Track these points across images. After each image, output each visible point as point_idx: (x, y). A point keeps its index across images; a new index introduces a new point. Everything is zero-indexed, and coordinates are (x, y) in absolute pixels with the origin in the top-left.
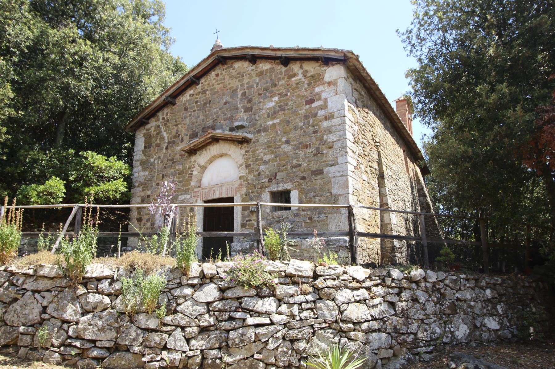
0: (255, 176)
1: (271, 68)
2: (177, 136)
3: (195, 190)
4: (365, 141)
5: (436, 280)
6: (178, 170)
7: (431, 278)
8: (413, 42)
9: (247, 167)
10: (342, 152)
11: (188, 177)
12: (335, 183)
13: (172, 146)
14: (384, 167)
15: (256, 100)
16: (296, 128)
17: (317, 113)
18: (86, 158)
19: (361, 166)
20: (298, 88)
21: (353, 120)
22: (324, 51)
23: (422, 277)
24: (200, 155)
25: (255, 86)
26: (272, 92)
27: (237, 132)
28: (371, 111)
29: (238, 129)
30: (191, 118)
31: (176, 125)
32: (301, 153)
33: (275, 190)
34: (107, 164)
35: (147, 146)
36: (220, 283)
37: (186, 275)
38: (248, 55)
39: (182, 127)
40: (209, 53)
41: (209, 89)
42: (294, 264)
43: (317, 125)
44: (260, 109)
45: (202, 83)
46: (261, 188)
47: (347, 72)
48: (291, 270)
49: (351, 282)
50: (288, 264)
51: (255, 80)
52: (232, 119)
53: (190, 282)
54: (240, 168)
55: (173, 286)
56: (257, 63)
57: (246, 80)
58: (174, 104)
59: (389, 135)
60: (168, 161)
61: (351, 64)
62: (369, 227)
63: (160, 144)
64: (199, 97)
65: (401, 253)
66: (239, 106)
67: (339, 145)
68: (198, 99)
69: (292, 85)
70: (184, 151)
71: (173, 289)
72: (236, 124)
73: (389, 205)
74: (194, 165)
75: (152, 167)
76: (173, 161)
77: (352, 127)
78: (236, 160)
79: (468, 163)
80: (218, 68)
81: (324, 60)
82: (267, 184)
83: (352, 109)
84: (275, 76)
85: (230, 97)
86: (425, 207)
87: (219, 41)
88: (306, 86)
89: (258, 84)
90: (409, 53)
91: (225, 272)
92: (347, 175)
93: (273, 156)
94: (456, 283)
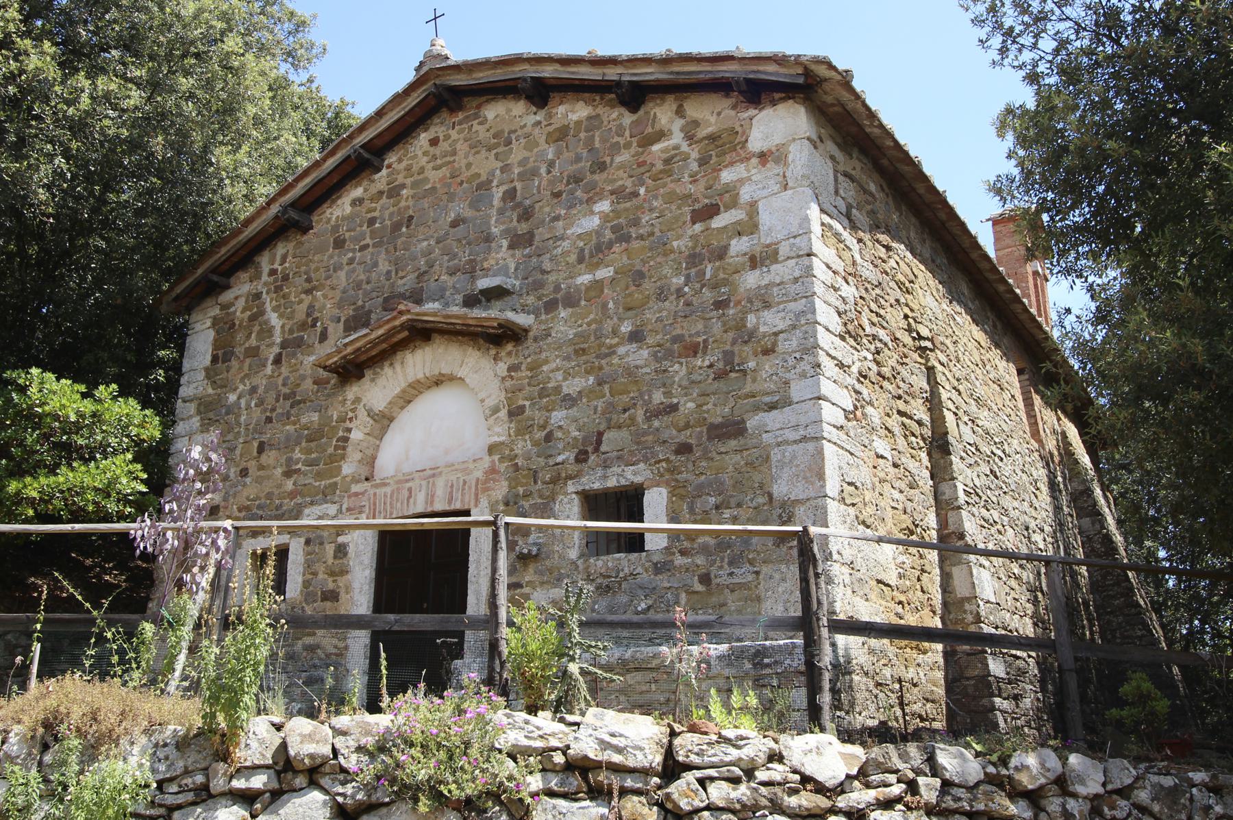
0: (536, 443)
1: (589, 118)
2: (309, 322)
3: (355, 488)
4: (882, 334)
5: (1101, 790)
7: (1082, 782)
8: (1008, 23)
9: (511, 414)
10: (804, 366)
11: (336, 448)
12: (782, 465)
13: (294, 355)
14: (949, 417)
15: (544, 210)
16: (661, 295)
17: (726, 248)
18: (23, 390)
19: (869, 410)
20: (669, 173)
21: (839, 265)
22: (744, 60)
23: (1051, 776)
24: (373, 380)
25: (543, 171)
26: (591, 187)
27: (486, 308)
28: (900, 241)
29: (488, 300)
30: (354, 271)
31: (308, 292)
32: (678, 371)
33: (596, 486)
34: (88, 406)
35: (222, 355)
36: (340, 789)
37: (225, 760)
38: (524, 79)
39: (325, 296)
40: (410, 76)
41: (408, 181)
42: (598, 724)
43: (725, 282)
44: (557, 239)
45: (389, 167)
46: (555, 480)
47: (818, 124)
48: (585, 746)
49: (794, 792)
50: (578, 724)
51: (543, 153)
52: (472, 270)
53: (238, 784)
54: (492, 420)
55: (181, 799)
56: (550, 104)
57: (517, 153)
58: (305, 229)
59: (964, 319)
60: (277, 400)
61: (829, 99)
62: (899, 609)
63: (258, 348)
64: (378, 206)
65: (1016, 698)
66: (494, 230)
67: (794, 343)
68: (376, 214)
69: (653, 165)
70: (325, 368)
71: (179, 807)
72: (484, 283)
73: (968, 539)
74: (353, 410)
75: (231, 418)
76: (295, 400)
77: (836, 290)
78: (482, 395)
79: (1198, 388)
80: (437, 121)
81: (744, 87)
82: (572, 468)
83: (837, 235)
84: (603, 141)
85: (471, 206)
86: (1100, 546)
87: (440, 42)
88: (694, 166)
89: (551, 164)
90: (998, 58)
91: (360, 749)
92: (818, 439)
93: (591, 379)
94: (1175, 803)
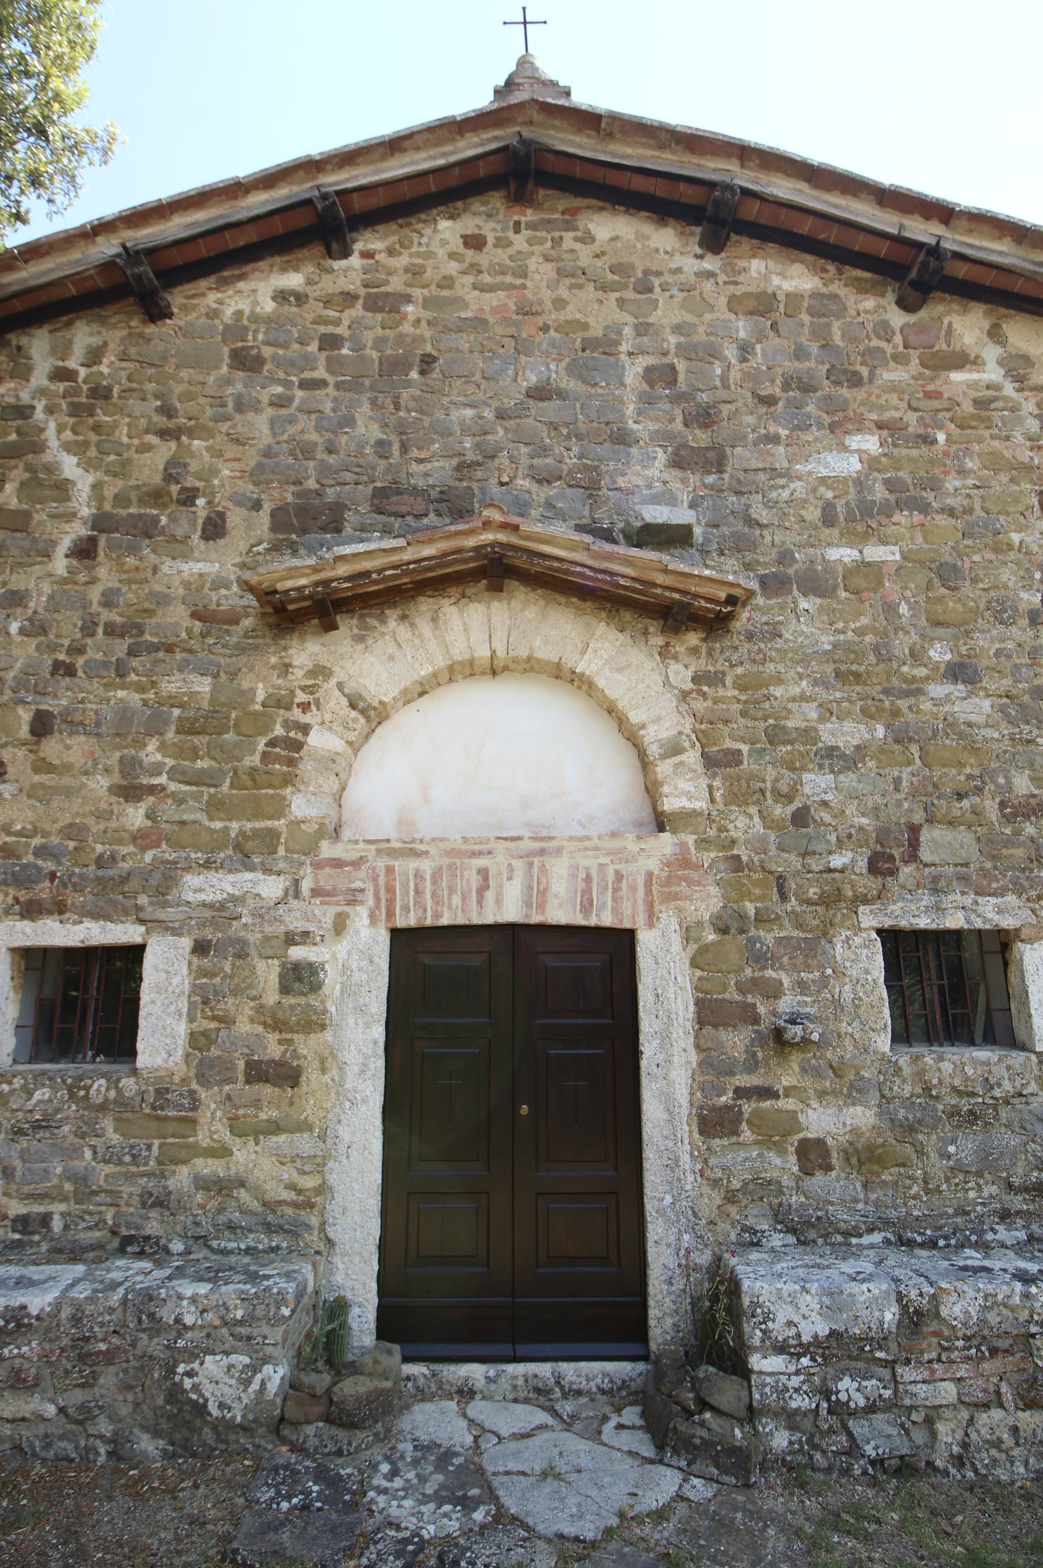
1: (815, 295)
6: (174, 702)
33: (923, 923)
40: (482, 99)
45: (367, 255)
68: (342, 330)
80: (477, 206)
